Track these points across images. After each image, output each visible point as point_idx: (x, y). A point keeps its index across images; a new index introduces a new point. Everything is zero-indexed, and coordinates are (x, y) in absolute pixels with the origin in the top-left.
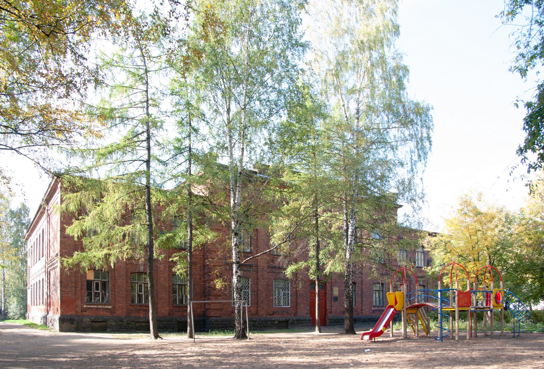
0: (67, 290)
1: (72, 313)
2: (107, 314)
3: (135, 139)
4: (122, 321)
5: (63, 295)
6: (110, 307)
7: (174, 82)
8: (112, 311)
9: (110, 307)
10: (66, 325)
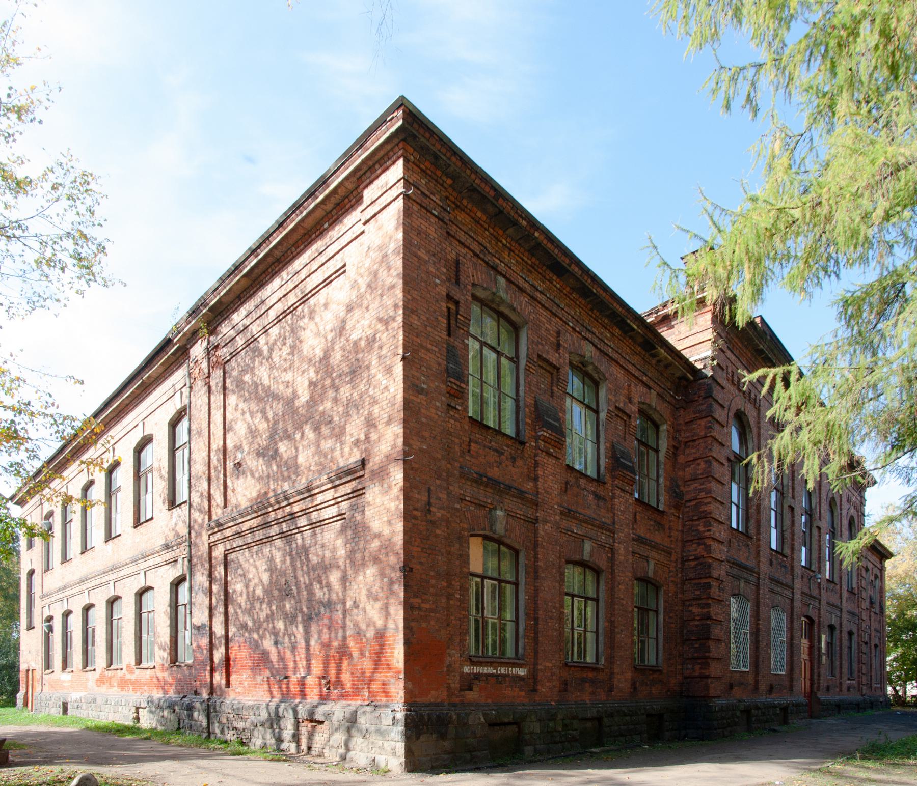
0: (423, 606)
1: (436, 695)
2: (516, 696)
3: (830, 428)
4: (553, 718)
5: (413, 624)
6: (523, 672)
7: (911, 482)
8: (531, 683)
9: (523, 672)
10: (427, 741)
